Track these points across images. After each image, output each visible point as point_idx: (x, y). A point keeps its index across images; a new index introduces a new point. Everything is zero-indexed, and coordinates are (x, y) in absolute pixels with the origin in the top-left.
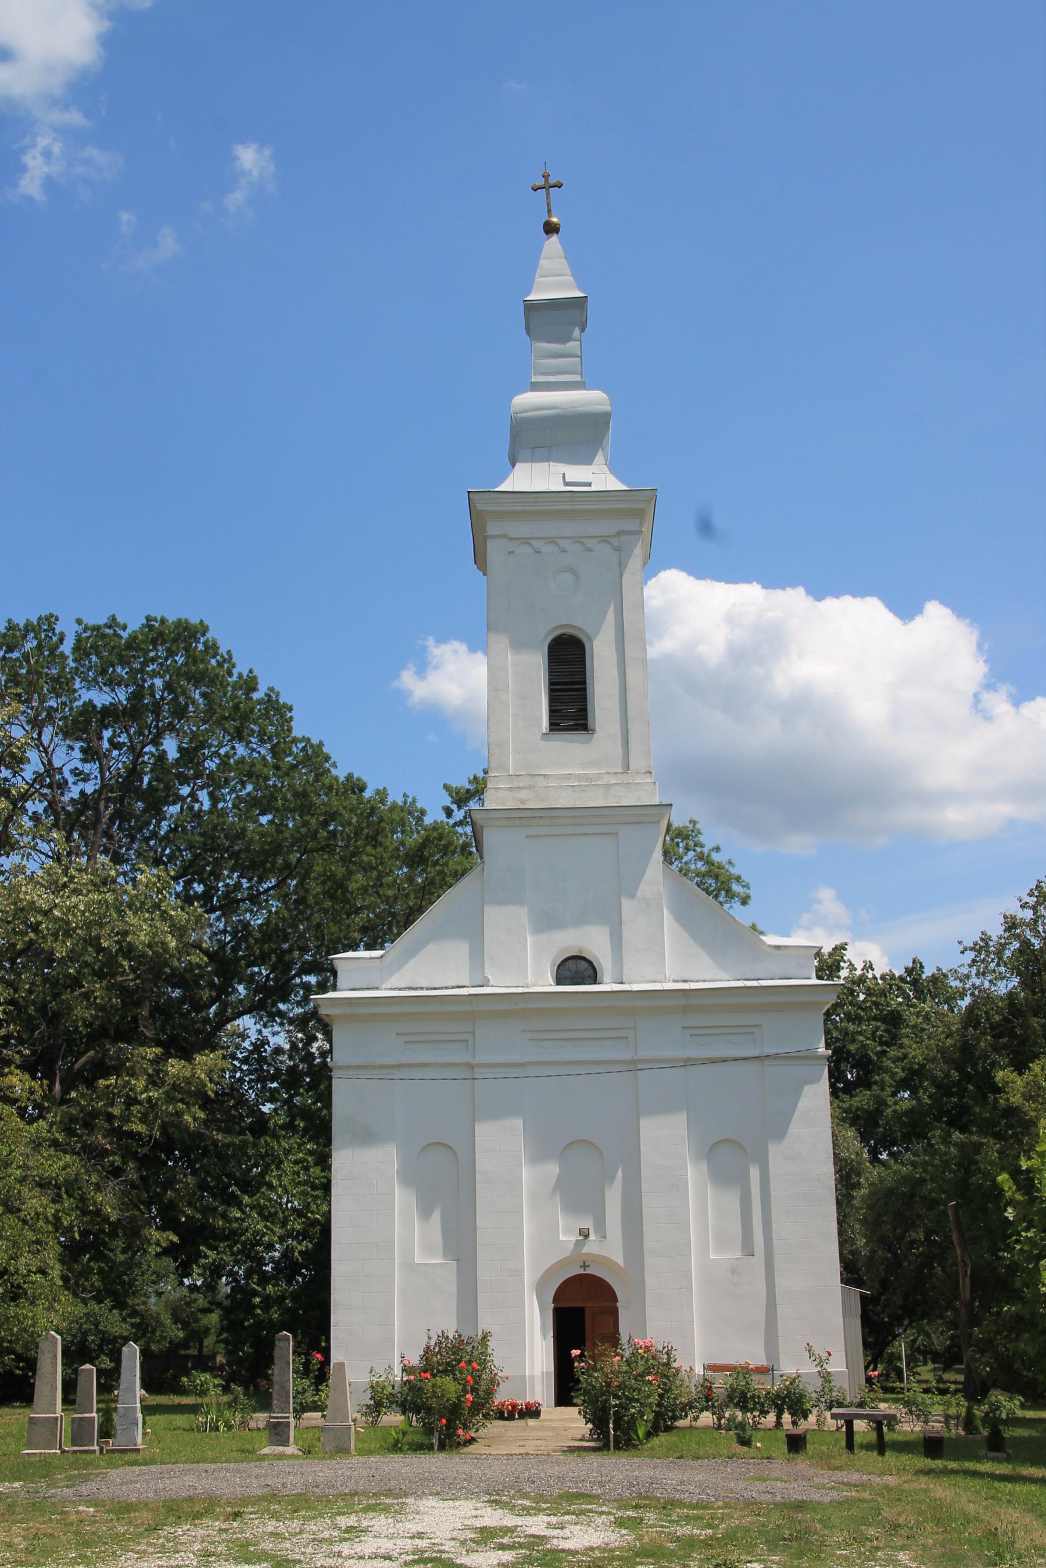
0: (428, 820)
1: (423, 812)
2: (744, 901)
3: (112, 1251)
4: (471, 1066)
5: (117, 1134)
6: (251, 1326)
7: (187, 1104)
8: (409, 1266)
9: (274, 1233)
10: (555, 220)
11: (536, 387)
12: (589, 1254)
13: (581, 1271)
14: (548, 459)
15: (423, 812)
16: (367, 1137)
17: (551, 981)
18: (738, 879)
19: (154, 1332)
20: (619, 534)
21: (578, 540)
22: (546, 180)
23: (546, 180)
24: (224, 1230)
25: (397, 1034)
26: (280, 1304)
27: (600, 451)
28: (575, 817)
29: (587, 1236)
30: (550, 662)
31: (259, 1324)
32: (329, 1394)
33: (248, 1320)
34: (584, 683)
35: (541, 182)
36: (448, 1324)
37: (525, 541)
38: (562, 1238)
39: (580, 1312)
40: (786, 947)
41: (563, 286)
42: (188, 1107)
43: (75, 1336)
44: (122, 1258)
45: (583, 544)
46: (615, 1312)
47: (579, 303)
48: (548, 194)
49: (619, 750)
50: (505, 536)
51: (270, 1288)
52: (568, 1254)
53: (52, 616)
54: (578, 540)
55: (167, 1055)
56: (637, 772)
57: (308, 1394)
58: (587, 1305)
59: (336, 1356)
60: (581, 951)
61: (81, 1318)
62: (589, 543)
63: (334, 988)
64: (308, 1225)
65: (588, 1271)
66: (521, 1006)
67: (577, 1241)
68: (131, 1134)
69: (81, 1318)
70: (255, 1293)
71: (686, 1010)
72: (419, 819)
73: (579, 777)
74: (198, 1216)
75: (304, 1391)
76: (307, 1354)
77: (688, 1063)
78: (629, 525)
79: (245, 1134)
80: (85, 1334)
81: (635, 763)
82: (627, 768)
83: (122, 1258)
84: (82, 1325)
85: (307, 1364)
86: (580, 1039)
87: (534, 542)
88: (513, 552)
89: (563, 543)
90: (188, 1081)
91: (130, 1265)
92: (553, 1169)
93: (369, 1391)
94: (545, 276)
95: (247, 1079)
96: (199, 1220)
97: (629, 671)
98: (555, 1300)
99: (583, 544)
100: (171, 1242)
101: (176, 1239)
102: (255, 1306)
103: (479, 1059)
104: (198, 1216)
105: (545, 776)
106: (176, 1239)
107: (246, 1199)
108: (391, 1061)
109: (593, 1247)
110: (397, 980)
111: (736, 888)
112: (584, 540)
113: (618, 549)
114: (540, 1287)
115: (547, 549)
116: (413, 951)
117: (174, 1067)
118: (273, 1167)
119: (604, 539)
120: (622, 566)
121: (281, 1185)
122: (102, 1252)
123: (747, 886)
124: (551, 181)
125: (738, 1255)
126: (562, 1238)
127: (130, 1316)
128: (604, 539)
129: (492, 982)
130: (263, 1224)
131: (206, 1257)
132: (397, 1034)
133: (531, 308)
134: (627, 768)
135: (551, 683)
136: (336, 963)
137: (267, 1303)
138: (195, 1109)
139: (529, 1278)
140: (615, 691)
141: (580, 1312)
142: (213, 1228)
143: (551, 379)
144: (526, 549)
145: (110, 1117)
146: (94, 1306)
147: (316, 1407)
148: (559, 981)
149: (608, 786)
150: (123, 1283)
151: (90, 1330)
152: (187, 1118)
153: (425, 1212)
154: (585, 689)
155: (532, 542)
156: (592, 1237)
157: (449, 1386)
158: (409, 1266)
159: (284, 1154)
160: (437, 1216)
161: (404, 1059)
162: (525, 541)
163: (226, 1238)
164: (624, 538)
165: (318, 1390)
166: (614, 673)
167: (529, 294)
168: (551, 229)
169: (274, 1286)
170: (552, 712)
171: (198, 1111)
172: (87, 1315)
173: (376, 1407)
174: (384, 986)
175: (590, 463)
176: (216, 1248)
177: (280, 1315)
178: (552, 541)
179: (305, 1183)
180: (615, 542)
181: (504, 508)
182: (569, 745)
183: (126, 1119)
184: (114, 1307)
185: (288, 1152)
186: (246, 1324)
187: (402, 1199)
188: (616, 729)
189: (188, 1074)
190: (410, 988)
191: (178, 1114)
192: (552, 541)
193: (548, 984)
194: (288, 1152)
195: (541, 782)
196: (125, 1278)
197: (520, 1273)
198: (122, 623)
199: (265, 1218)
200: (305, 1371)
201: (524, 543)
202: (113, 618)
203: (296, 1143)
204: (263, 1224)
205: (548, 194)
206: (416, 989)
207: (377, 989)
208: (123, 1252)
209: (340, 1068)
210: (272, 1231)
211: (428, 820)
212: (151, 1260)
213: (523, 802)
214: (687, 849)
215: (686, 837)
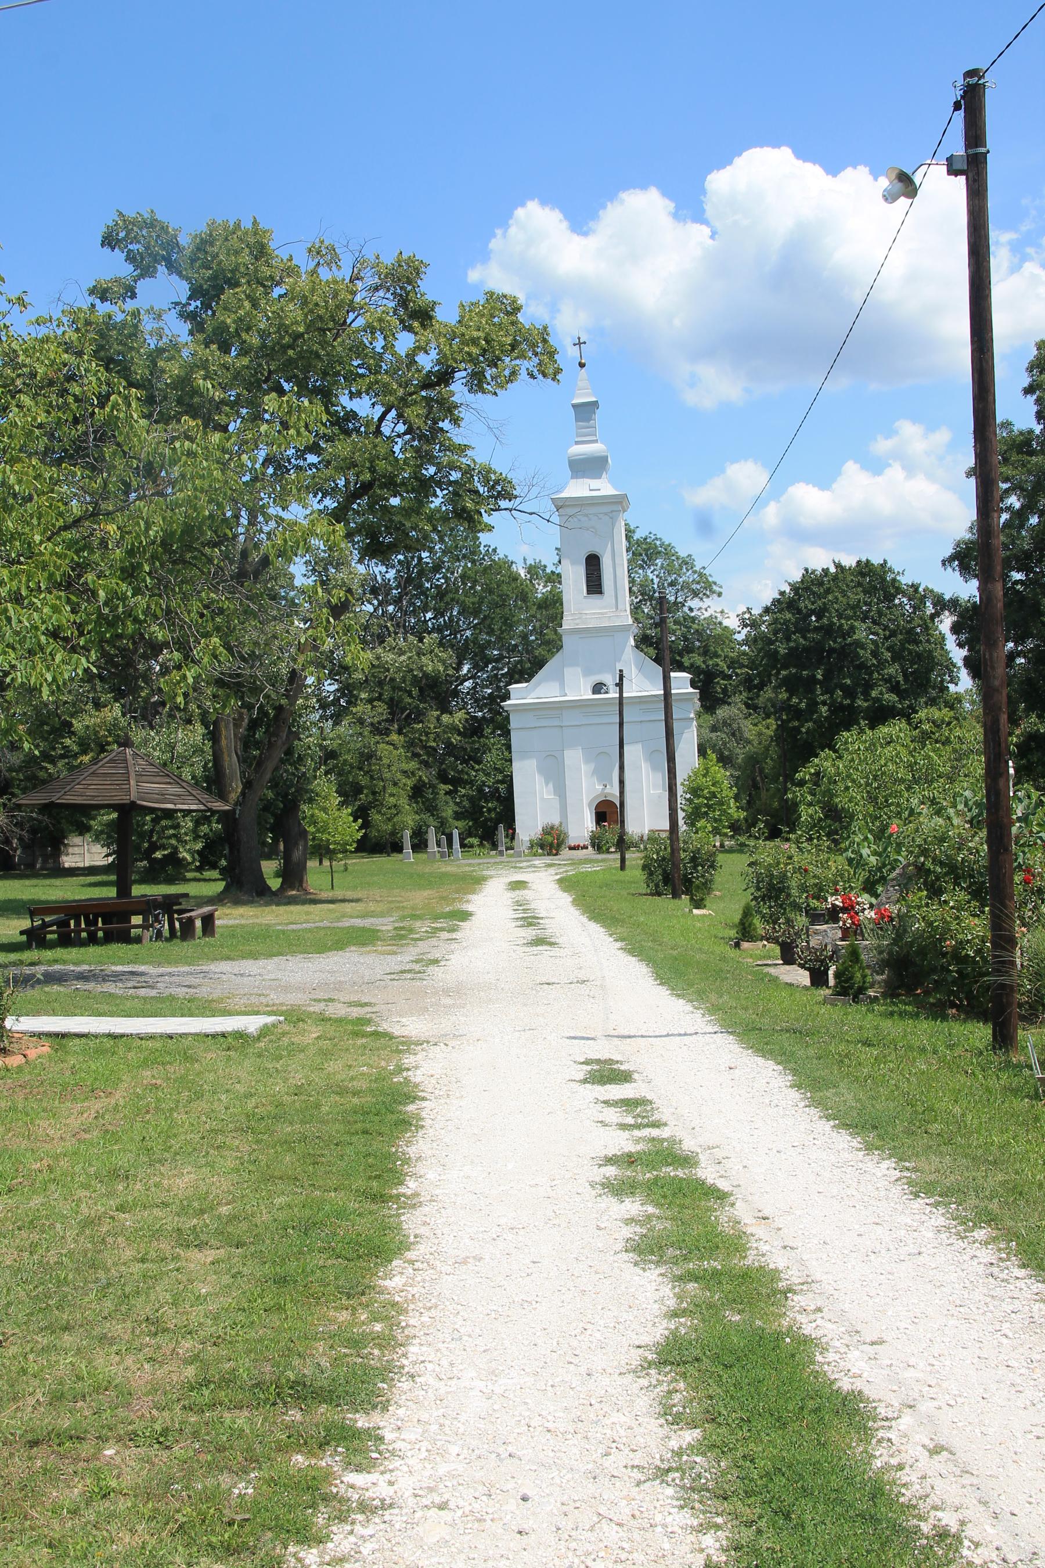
0: (548, 571)
1: (545, 566)
2: (720, 595)
5: (425, 747)
8: (542, 799)
15: (545, 566)
16: (525, 755)
17: (590, 692)
18: (715, 583)
21: (595, 515)
31: (487, 820)
32: (515, 843)
36: (555, 820)
41: (588, 395)
47: (595, 405)
54: (595, 515)
55: (442, 713)
62: (601, 516)
68: (430, 747)
70: (484, 807)
71: (640, 703)
78: (615, 508)
82: (617, 608)
91: (434, 799)
92: (592, 766)
107: (477, 767)
108: (533, 726)
109: (608, 790)
110: (533, 695)
111: (715, 588)
114: (590, 805)
116: (539, 684)
119: (606, 514)
123: (721, 587)
128: (606, 514)
134: (617, 608)
137: (489, 810)
139: (585, 802)
142: (462, 779)
145: (421, 741)
147: (512, 849)
148: (594, 693)
153: (547, 784)
158: (542, 799)
160: (551, 786)
168: (582, 365)
173: (532, 847)
182: (595, 599)
183: (427, 741)
185: (493, 745)
187: (539, 779)
194: (493, 745)
195: (584, 617)
200: (507, 836)
211: (548, 571)
214: (688, 570)
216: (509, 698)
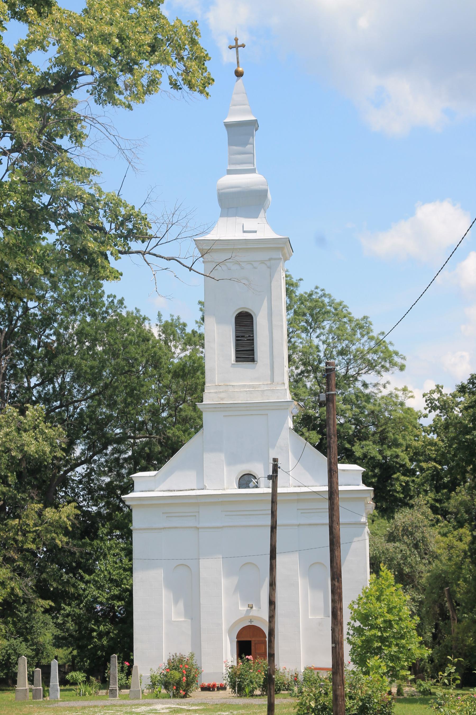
0: (188, 330)
2: (402, 368)
3: (20, 611)
4: (198, 528)
5: (21, 550)
6: (91, 648)
7: (57, 533)
9: (104, 597)
10: (240, 69)
12: (253, 616)
13: (249, 624)
14: (235, 215)
17: (236, 486)
18: (396, 353)
19: (42, 653)
20: (270, 259)
22: (237, 42)
23: (237, 42)
24: (74, 594)
26: (107, 636)
27: (262, 211)
28: (247, 407)
29: (252, 608)
30: (236, 326)
32: (132, 680)
33: (90, 645)
35: (234, 44)
38: (240, 608)
39: (249, 643)
40: (347, 470)
42: (58, 536)
43: (4, 656)
44: (26, 615)
45: (252, 264)
47: (253, 125)
48: (237, 52)
49: (269, 372)
51: (102, 628)
52: (243, 616)
55: (45, 507)
56: (278, 384)
57: (123, 680)
58: (252, 639)
59: (136, 663)
61: (7, 647)
64: (122, 591)
65: (253, 624)
66: (220, 500)
69: (7, 647)
70: (94, 630)
71: (298, 501)
72: (183, 330)
73: (249, 386)
74: (60, 587)
75: (122, 679)
76: (123, 664)
77: (299, 525)
79: (85, 539)
80: (9, 655)
81: (276, 379)
82: (273, 381)
83: (26, 615)
84: (7, 651)
85: (122, 668)
90: (57, 522)
91: (29, 619)
92: (235, 580)
93: (150, 679)
94: (235, 105)
95: (82, 493)
96: (60, 589)
97: (274, 331)
98: (238, 636)
99: (252, 264)
100: (51, 606)
101: (53, 604)
102: (93, 637)
103: (201, 525)
104: (60, 587)
106: (53, 604)
109: (254, 612)
110: (163, 486)
111: (396, 359)
113: (269, 267)
114: (230, 632)
117: (49, 513)
118: (101, 557)
119: (262, 262)
120: (271, 276)
121: (106, 570)
122: (15, 612)
124: (240, 43)
125: (322, 617)
126: (240, 608)
127: (31, 645)
128: (262, 262)
129: (207, 488)
130: (97, 592)
131: (64, 609)
133: (228, 125)
134: (273, 381)
136: (133, 479)
138: (61, 536)
139: (225, 627)
140: (267, 342)
141: (249, 643)
142: (67, 593)
146: (12, 640)
149: (263, 391)
150: (26, 628)
151: (12, 653)
152: (58, 541)
153: (176, 602)
154: (253, 340)
156: (254, 608)
157: (177, 675)
159: (108, 549)
163: (77, 599)
165: (127, 678)
166: (267, 333)
167: (226, 118)
168: (239, 74)
169: (104, 626)
170: (237, 351)
171: (63, 537)
172: (10, 645)
173: (153, 685)
174: (158, 489)
175: (257, 217)
176: (69, 605)
177: (108, 642)
179: (120, 568)
184: (23, 641)
185: (110, 549)
186: (89, 647)
188: (268, 361)
189: (57, 518)
190: (169, 491)
191: (53, 539)
194: (110, 549)
195: (231, 389)
196: (28, 626)
197: (220, 625)
199: (98, 588)
203: (115, 543)
204: (97, 592)
205: (237, 52)
206: (171, 491)
207: (153, 491)
208: (26, 612)
209: (136, 529)
210: (102, 595)
211: (188, 330)
212: (39, 615)
213: (222, 399)
214: (363, 336)
215: (361, 327)
216: (132, 490)
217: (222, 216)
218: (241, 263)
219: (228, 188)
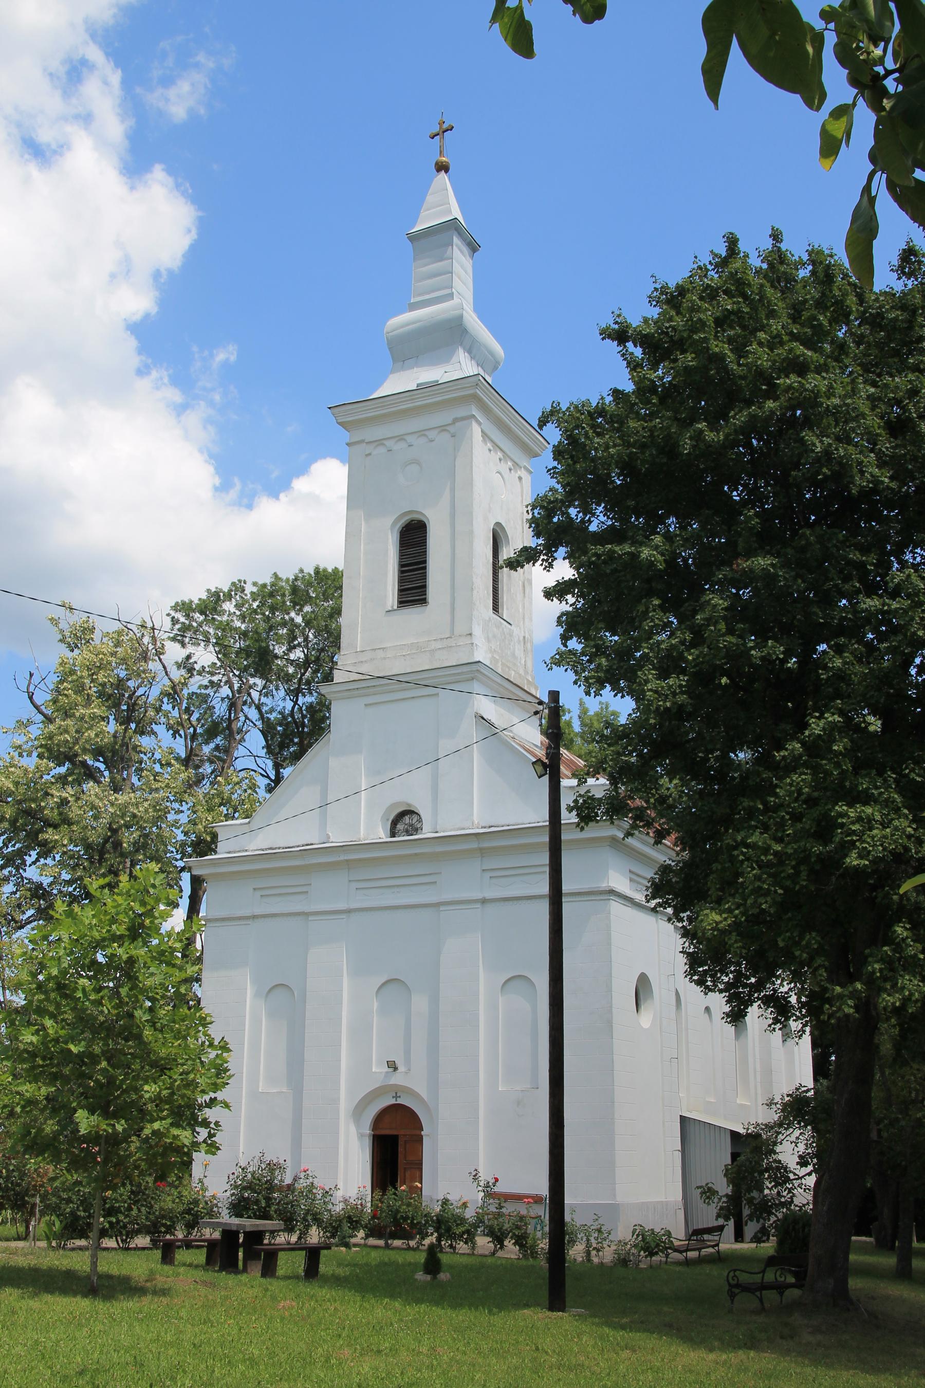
11: (413, 307)
13: (393, 1102)
20: (456, 420)
21: (421, 433)
25: (254, 889)
34: (425, 562)
35: (436, 129)
37: (379, 442)
46: (420, 1140)
50: (362, 441)
53: (240, 581)
54: (421, 433)
60: (409, 805)
62: (432, 434)
63: (216, 852)
65: (399, 1101)
66: (342, 858)
67: (387, 1072)
77: (484, 901)
78: (461, 412)
86: (398, 886)
87: (387, 443)
88: (370, 454)
89: (410, 439)
94: (428, 210)
105: (383, 649)
108: (247, 912)
112: (426, 433)
115: (398, 447)
119: (443, 428)
124: (445, 126)
128: (443, 428)
132: (254, 889)
133: (414, 238)
135: (401, 566)
139: (345, 1104)
143: (427, 297)
144: (382, 450)
149: (433, 651)
154: (425, 568)
155: (385, 442)
161: (258, 911)
162: (379, 442)
164: (458, 424)
168: (442, 167)
178: (400, 438)
180: (452, 429)
181: (360, 417)
182: (413, 614)
190: (271, 849)
192: (400, 438)
193: (382, 834)
195: (380, 654)
197: (336, 1101)
198: (285, 578)
201: (378, 445)
202: (275, 575)
217: (415, 259)
218: (405, 437)
219: (402, 327)
